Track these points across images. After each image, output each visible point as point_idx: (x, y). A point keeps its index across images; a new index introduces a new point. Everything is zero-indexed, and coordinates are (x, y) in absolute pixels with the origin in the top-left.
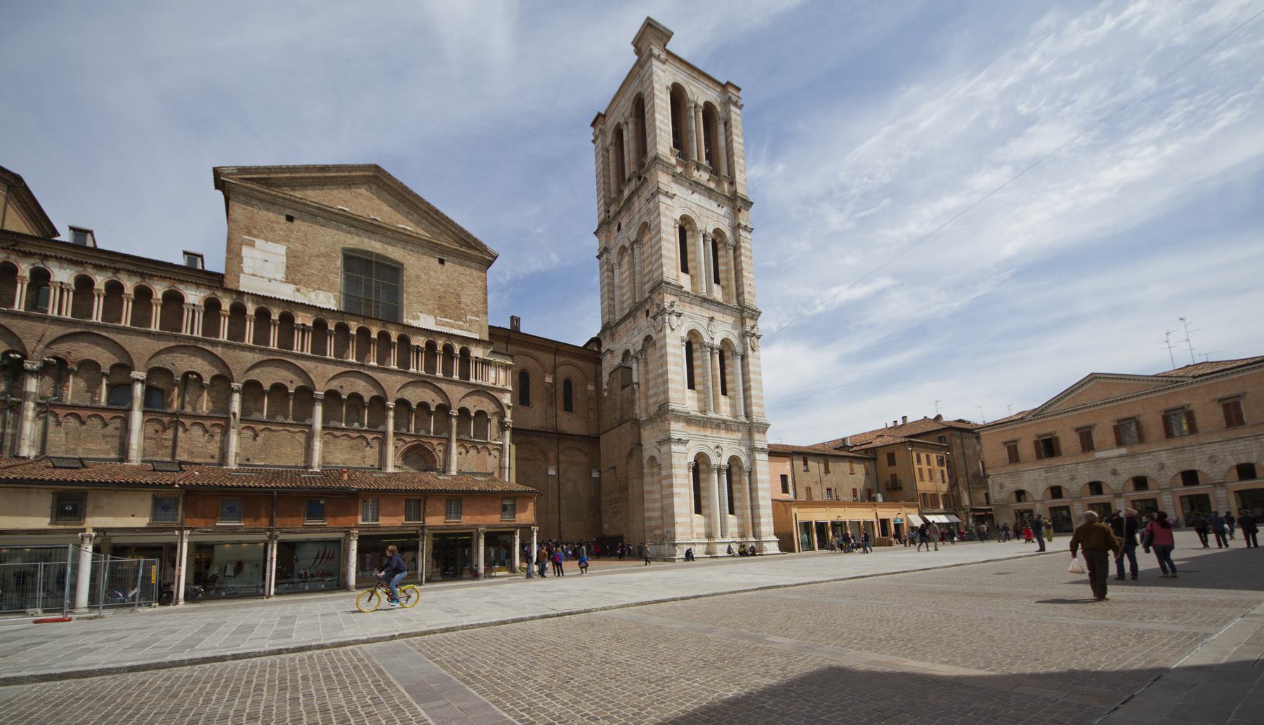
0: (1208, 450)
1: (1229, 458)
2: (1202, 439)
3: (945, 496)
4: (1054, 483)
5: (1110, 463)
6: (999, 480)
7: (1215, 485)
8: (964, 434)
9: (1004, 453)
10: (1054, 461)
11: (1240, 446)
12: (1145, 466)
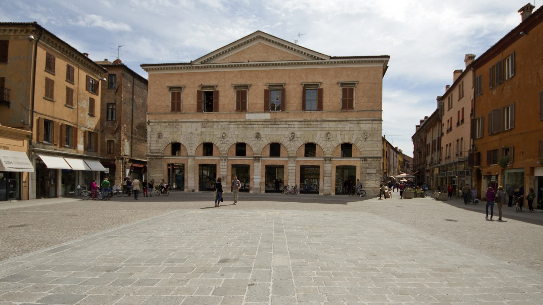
0: (327, 126)
1: (339, 136)
2: (324, 116)
3: (90, 136)
4: (208, 139)
5: (256, 126)
6: (158, 128)
7: (326, 159)
8: (137, 82)
9: (168, 99)
10: (211, 116)
11: (348, 127)
12: (279, 133)
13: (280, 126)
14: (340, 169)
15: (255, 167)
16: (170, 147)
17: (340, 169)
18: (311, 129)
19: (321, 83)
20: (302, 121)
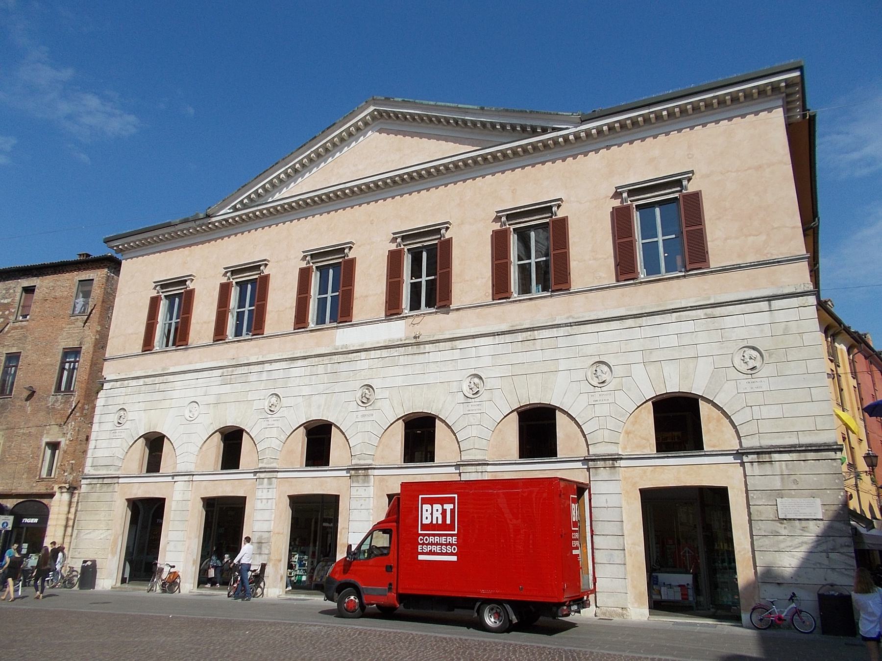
0: (593, 340)
1: (639, 371)
13: (432, 357)
14: (658, 505)
15: (354, 504)
16: (399, 433)
17: (658, 505)
18: (538, 356)
19: (559, 202)
20: (503, 333)
